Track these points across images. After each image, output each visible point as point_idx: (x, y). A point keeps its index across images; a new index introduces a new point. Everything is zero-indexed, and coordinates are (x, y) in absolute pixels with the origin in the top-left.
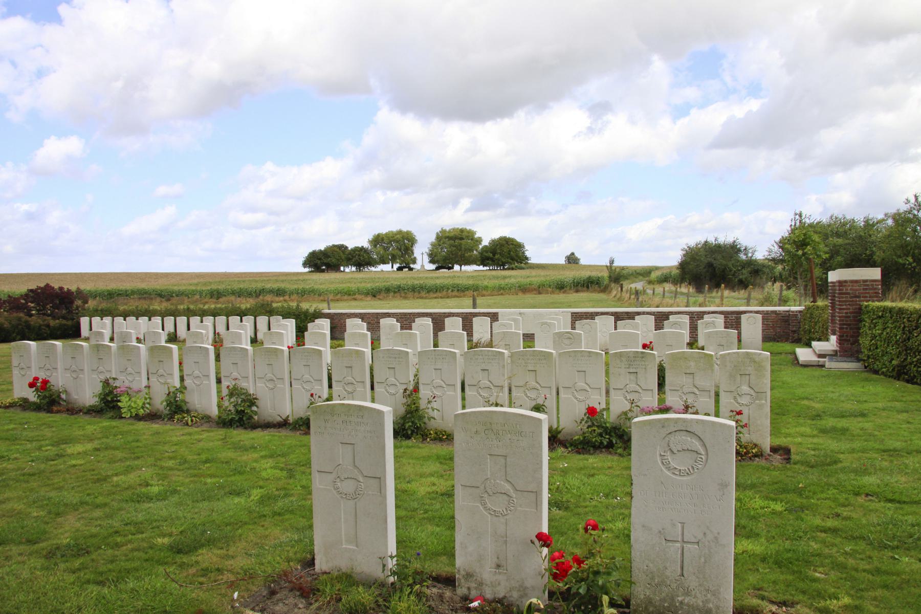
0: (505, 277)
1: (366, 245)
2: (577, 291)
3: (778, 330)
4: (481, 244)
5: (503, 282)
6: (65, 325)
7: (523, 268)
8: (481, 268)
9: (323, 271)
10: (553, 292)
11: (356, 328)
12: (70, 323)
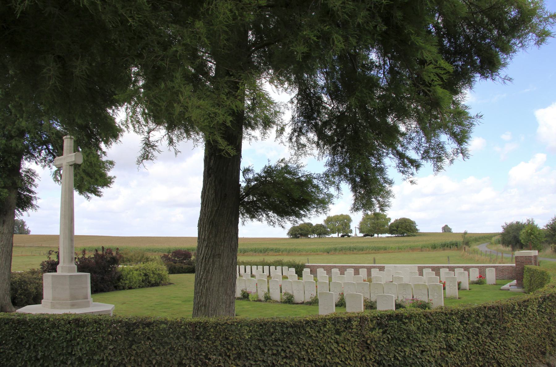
0: (403, 242)
1: (323, 223)
2: (444, 250)
3: (513, 274)
4: (390, 222)
5: (401, 245)
6: (189, 267)
7: (414, 236)
8: (390, 235)
9: (298, 237)
10: (429, 251)
11: (321, 272)
12: (191, 267)
